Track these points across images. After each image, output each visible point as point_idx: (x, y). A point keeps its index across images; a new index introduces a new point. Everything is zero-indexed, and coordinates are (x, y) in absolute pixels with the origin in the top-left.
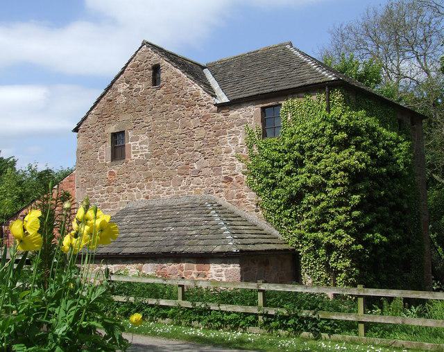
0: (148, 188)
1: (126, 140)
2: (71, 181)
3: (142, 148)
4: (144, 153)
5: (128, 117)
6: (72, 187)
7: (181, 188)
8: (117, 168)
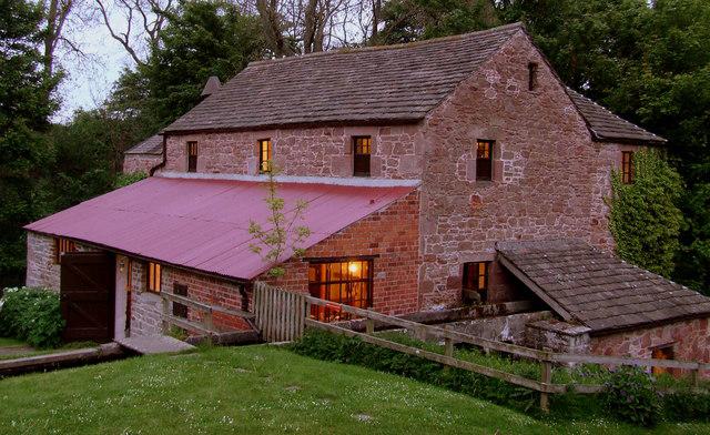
2: (413, 203)
3: (516, 170)
4: (518, 177)
5: (502, 123)
6: (413, 212)
8: (485, 192)
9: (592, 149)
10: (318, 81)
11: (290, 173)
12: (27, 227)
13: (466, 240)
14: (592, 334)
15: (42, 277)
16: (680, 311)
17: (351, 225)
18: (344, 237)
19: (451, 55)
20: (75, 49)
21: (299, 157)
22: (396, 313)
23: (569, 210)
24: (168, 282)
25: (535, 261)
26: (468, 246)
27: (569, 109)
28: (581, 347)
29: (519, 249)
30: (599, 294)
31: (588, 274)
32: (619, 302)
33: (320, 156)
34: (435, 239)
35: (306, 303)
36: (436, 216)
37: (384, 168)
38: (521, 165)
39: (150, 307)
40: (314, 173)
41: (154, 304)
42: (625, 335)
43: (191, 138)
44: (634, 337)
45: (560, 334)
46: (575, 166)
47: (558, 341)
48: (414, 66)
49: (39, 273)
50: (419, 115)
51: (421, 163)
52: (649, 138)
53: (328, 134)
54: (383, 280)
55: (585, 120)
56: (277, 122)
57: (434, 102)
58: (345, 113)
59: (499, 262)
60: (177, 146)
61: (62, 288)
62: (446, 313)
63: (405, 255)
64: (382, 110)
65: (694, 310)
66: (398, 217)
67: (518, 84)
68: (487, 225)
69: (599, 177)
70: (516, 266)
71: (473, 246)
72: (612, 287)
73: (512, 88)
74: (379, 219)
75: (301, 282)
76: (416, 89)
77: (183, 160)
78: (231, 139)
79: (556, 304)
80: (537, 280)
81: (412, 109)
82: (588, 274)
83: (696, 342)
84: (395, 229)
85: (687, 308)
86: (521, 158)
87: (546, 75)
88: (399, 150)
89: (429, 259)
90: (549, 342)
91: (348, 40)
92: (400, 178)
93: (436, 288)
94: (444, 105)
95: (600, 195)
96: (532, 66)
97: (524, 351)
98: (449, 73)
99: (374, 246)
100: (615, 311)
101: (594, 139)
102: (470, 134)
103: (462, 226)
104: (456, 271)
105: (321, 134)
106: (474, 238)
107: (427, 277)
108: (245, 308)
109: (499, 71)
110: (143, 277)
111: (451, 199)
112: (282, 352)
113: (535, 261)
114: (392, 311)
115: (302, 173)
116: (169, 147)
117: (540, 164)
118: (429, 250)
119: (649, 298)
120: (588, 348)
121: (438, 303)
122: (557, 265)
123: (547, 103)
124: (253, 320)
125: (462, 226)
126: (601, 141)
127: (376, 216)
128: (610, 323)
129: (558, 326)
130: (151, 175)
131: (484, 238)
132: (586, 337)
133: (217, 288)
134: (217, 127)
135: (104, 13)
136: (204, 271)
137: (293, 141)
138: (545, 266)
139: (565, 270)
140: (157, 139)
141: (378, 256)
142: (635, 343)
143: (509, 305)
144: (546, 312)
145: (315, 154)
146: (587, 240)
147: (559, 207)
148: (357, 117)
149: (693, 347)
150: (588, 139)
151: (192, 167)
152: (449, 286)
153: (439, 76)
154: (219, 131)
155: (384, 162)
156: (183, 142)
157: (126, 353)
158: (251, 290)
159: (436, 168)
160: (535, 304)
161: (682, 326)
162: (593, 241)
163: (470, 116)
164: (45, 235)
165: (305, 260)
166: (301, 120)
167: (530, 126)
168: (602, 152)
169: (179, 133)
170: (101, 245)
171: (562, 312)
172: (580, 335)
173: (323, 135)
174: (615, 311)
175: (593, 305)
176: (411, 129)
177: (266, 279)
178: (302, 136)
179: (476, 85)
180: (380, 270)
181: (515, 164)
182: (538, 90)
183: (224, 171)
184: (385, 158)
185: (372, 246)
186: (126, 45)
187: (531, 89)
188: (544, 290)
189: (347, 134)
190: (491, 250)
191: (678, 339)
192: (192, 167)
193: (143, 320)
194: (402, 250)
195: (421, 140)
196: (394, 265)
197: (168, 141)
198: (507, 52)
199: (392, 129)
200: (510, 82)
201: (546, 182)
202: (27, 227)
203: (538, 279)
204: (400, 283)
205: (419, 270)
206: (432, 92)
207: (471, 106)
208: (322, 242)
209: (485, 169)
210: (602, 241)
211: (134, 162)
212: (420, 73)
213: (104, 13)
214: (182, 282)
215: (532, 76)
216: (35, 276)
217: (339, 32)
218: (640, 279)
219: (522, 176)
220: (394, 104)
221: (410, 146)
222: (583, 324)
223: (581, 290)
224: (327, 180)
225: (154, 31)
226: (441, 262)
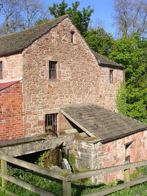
0: (71, 98)
2: (19, 88)
6: (19, 92)
47: (88, 146)
83: (140, 140)
92: (14, 78)
104: (42, 118)
107: (27, 121)
120: (100, 148)
194: (14, 109)
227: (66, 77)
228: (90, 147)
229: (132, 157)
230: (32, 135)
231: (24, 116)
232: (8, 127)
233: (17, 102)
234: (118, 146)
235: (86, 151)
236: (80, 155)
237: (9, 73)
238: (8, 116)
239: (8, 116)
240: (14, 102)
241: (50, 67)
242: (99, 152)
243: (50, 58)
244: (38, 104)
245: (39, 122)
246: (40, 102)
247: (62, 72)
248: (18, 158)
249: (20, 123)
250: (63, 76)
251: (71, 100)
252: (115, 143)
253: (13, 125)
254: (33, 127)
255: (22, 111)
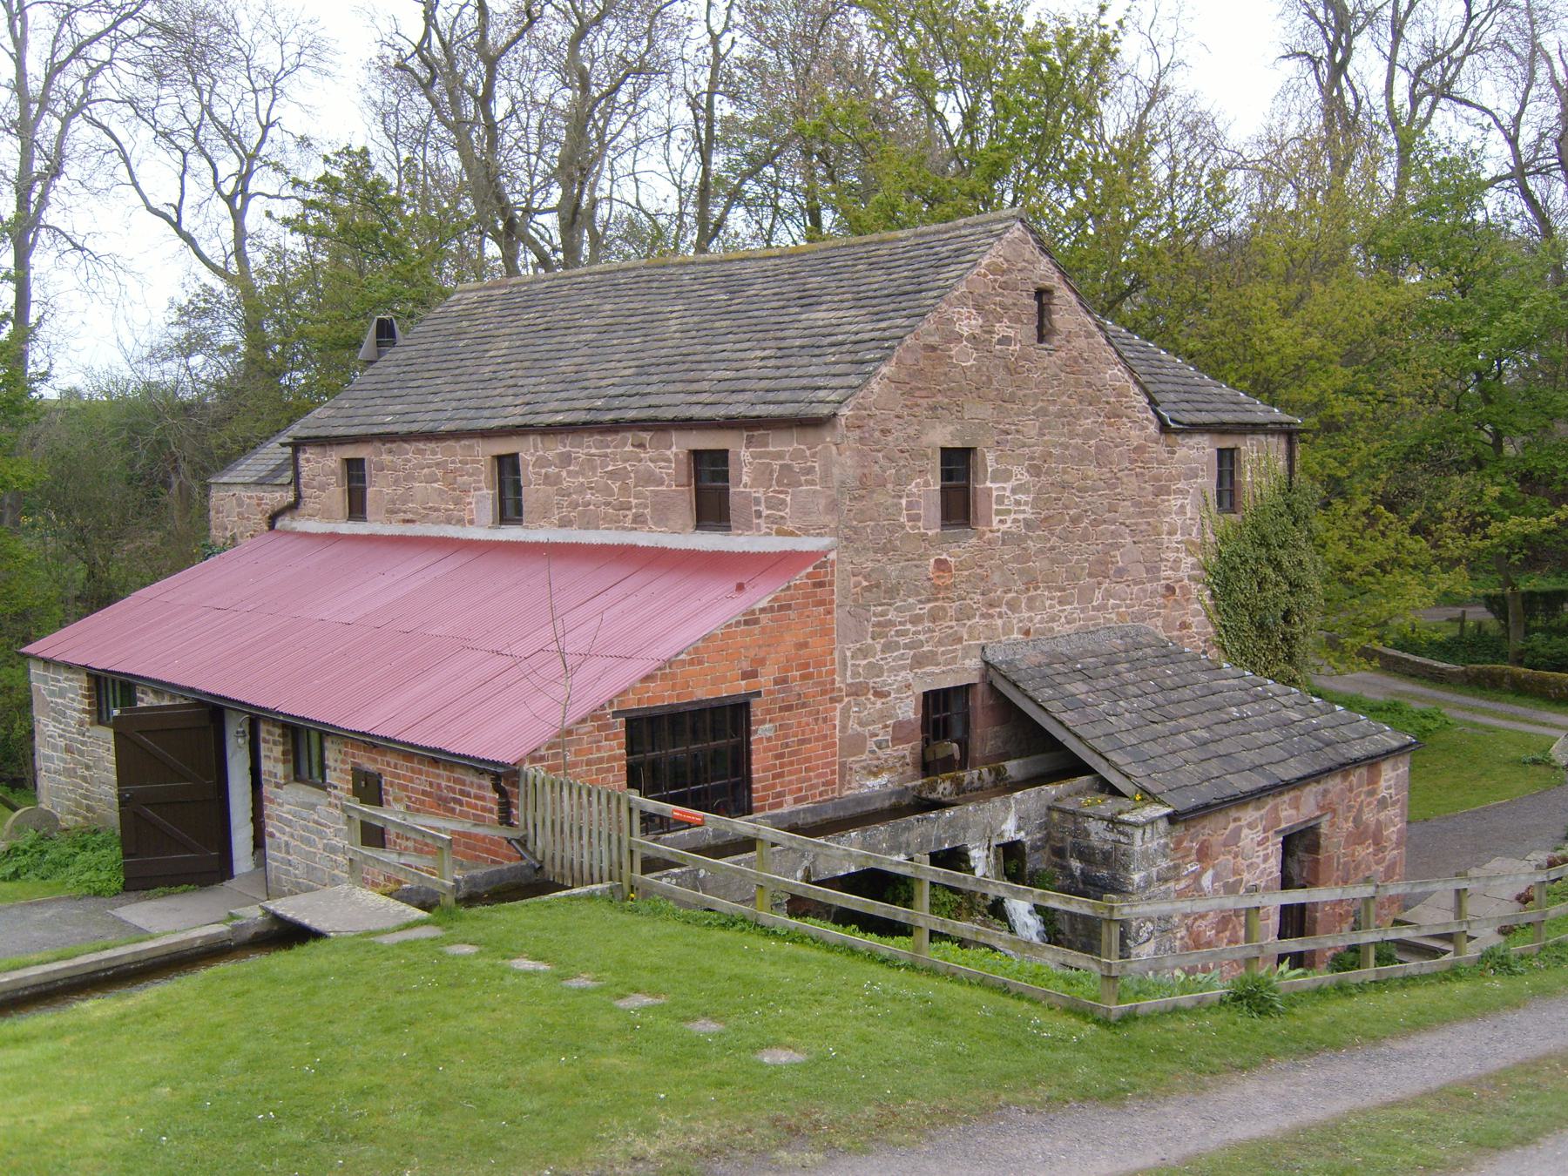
0: (1030, 609)
1: (981, 475)
2: (821, 584)
3: (1018, 503)
4: (1021, 516)
5: (985, 411)
6: (821, 603)
7: (1094, 608)
8: (962, 548)
9: (1159, 450)
10: (606, 330)
11: (564, 523)
12: (27, 649)
13: (925, 649)
14: (1172, 819)
15: (68, 749)
16: (1329, 757)
17: (704, 639)
18: (692, 662)
19: (879, 275)
20: (76, 246)
21: (581, 489)
22: (797, 801)
23: (1120, 572)
24: (339, 765)
25: (1058, 679)
26: (930, 658)
27: (1116, 374)
28: (1153, 845)
29: (1028, 657)
30: (1182, 737)
31: (1159, 698)
32: (1221, 748)
33: (625, 489)
34: (864, 652)
35: (630, 810)
36: (866, 607)
37: (759, 514)
38: (1027, 491)
39: (305, 813)
40: (615, 523)
41: (313, 807)
42: (1234, 813)
43: (351, 452)
44: (1249, 814)
45: (1113, 822)
46: (1130, 485)
47: (1110, 836)
48: (808, 300)
49: (62, 743)
50: (825, 410)
51: (833, 506)
52: (1271, 418)
53: (641, 446)
54: (769, 739)
55: (1148, 394)
56: (529, 420)
57: (854, 380)
58: (674, 404)
59: (992, 687)
60: (322, 467)
61: (121, 781)
62: (892, 793)
63: (810, 688)
64: (747, 396)
65: (1357, 751)
66: (792, 614)
67: (1016, 332)
68: (964, 615)
69: (1174, 502)
70: (1024, 693)
71: (941, 659)
72: (1209, 718)
73: (1005, 340)
74: (756, 622)
75: (612, 758)
76: (813, 349)
77: (337, 495)
78: (435, 453)
79: (1083, 748)
80: (1064, 717)
81: (810, 395)
82: (1159, 698)
83: (1360, 811)
84: (790, 639)
85: (1343, 749)
86: (1026, 477)
87: (1068, 313)
88: (788, 477)
89: (857, 691)
90: (1093, 837)
91: (645, 204)
92: (792, 534)
93: (871, 745)
94: (874, 385)
95: (1178, 537)
96: (1042, 294)
97: (1068, 902)
98: (879, 316)
99: (749, 675)
100: (1214, 768)
101: (1164, 428)
102: (925, 440)
103: (916, 620)
104: (909, 710)
105: (623, 445)
106: (940, 643)
107: (853, 727)
108: (506, 818)
109: (979, 308)
110: (284, 753)
111: (893, 570)
112: (585, 909)
113: (1058, 679)
114: (789, 798)
115: (589, 523)
116: (306, 469)
117: (1064, 486)
118: (855, 674)
119: (1275, 735)
120: (1166, 845)
121: (875, 775)
122: (1101, 684)
123: (1074, 365)
124: (523, 842)
125: (916, 620)
126: (1177, 432)
127: (750, 620)
128: (1207, 794)
129: (1108, 806)
130: (272, 527)
131: (960, 640)
132: (1162, 825)
133: (443, 778)
134: (404, 428)
135: (126, 161)
136: (412, 745)
137: (566, 459)
138: (1078, 688)
139: (1116, 694)
140: (273, 453)
141: (758, 694)
142: (1251, 826)
143: (1013, 768)
144: (1083, 781)
145: (615, 487)
146: (1156, 626)
147: (1102, 568)
148: (696, 412)
149: (1355, 821)
150: (1153, 429)
151: (357, 509)
152: (896, 740)
153: (857, 324)
154: (409, 437)
155: (757, 501)
156: (333, 460)
157: (288, 935)
158: (515, 784)
159: (862, 512)
160: (1072, 767)
161: (1335, 784)
162: (1166, 628)
163: (924, 402)
164: (69, 667)
165: (616, 714)
166: (583, 417)
167: (1042, 412)
168: (1181, 452)
169: (324, 442)
170: (191, 690)
171: (1115, 779)
172: (1152, 822)
173: (629, 448)
174: (1214, 768)
175: (1177, 761)
176: (811, 435)
177: (542, 758)
178: (587, 448)
179: (934, 340)
180: (763, 722)
181: (1014, 491)
182: (1056, 340)
183: (424, 518)
184: (759, 493)
185: (747, 675)
186: (177, 226)
187: (1041, 339)
188: (1079, 737)
189: (679, 446)
190: (974, 663)
191: (1327, 808)
192: (357, 509)
193: (301, 839)
194: (803, 677)
195: (837, 456)
196: (789, 708)
197: (302, 456)
198: (994, 269)
199: (772, 436)
200: (1001, 329)
201: (1075, 521)
202: (27, 649)
203: (1072, 714)
204: (802, 742)
205: (838, 713)
206: (849, 358)
207: (927, 384)
208: (648, 678)
209: (958, 505)
210: (1184, 626)
211: (235, 499)
212: (820, 316)
213: (126, 161)
214: (370, 767)
215: (1043, 312)
216: (54, 747)
217: (627, 191)
218: (1257, 698)
219: (1028, 513)
220: (772, 384)
221: (810, 470)
222: (1161, 802)
223: (1148, 731)
224: (642, 538)
225: (234, 194)
226: (878, 694)
227: (1013, 516)
228: (1122, 839)
229: (1253, 1029)
230: (875, 783)
231: (839, 706)
232: (781, 756)
233: (817, 646)
234: (1249, 837)
235: (1107, 856)
236: (1078, 873)
237: (766, 512)
238: (781, 709)
239: (781, 709)
240: (805, 645)
241: (947, 475)
242: (1164, 864)
243: (943, 435)
244: (897, 646)
245: (899, 726)
246: (902, 640)
247: (995, 493)
248: (1431, 894)
249: (825, 737)
250: (998, 512)
251: (1031, 620)
252: (1232, 826)
253: (802, 742)
254: (873, 752)
255: (833, 682)
